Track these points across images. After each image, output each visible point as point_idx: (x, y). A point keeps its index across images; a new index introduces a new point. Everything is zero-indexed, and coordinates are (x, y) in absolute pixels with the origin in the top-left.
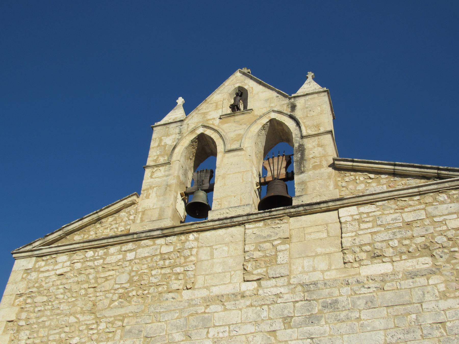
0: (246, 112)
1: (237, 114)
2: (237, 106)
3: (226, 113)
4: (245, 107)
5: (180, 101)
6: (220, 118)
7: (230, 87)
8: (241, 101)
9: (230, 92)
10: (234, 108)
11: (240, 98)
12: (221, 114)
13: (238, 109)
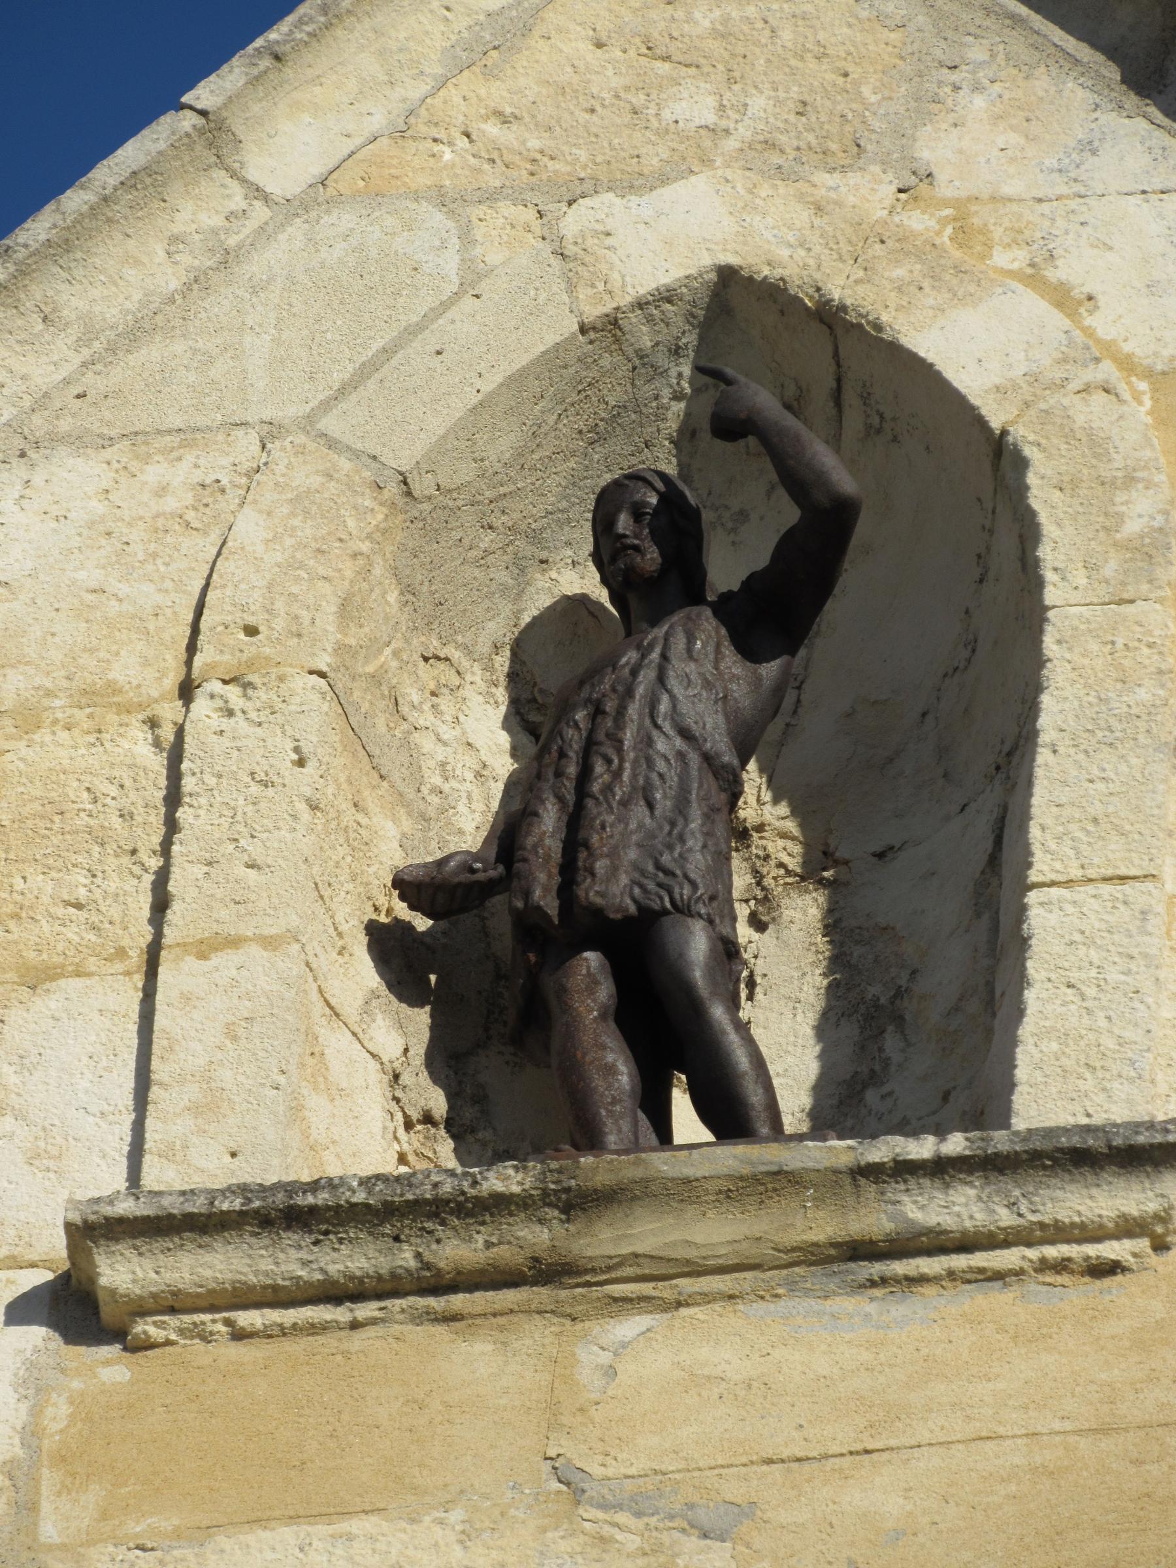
0: (961, 1206)
1: (648, 1233)
2: (635, 944)
3: (276, 1165)
4: (929, 1020)
5: (422, 923)
6: (73, 1308)
7: (428, 244)
8: (758, 802)
9: (420, 419)
10: (542, 989)
11: (744, 680)
12: (102, 1180)
13: (680, 1043)
